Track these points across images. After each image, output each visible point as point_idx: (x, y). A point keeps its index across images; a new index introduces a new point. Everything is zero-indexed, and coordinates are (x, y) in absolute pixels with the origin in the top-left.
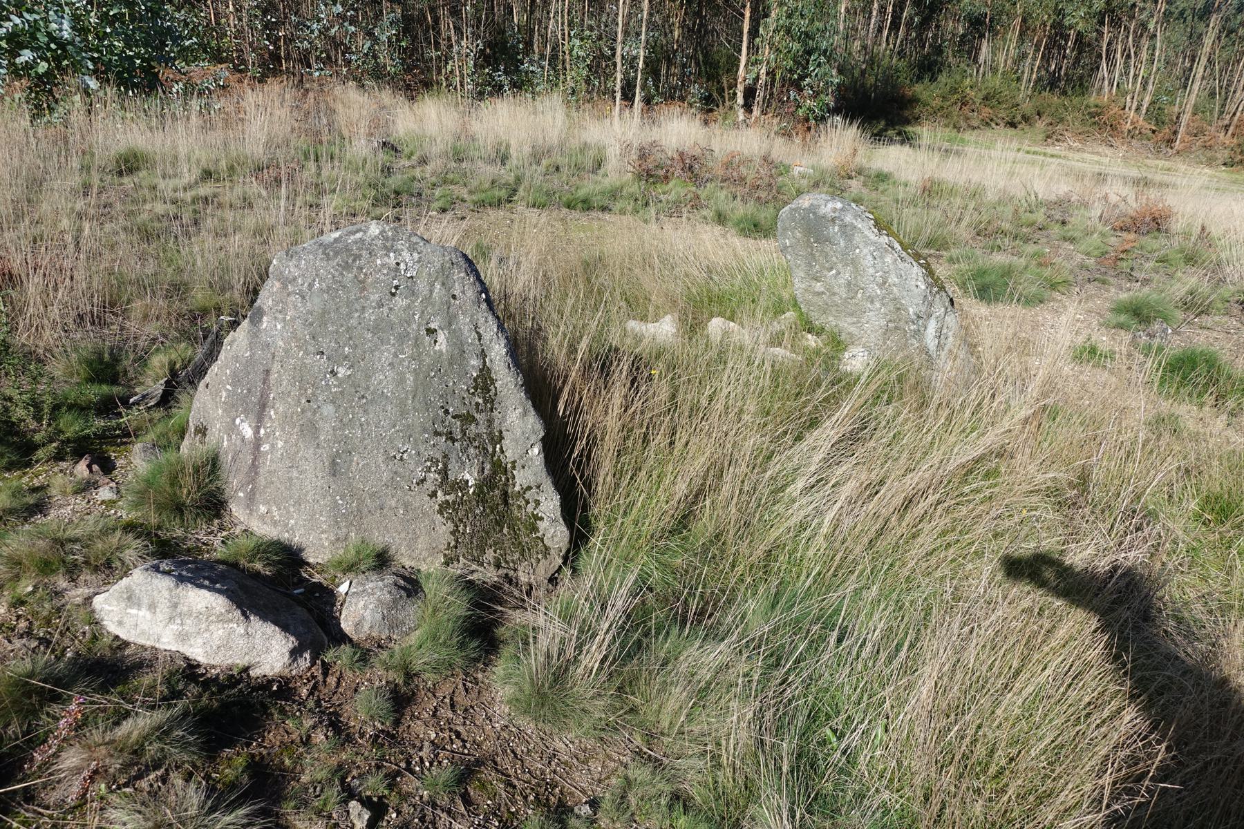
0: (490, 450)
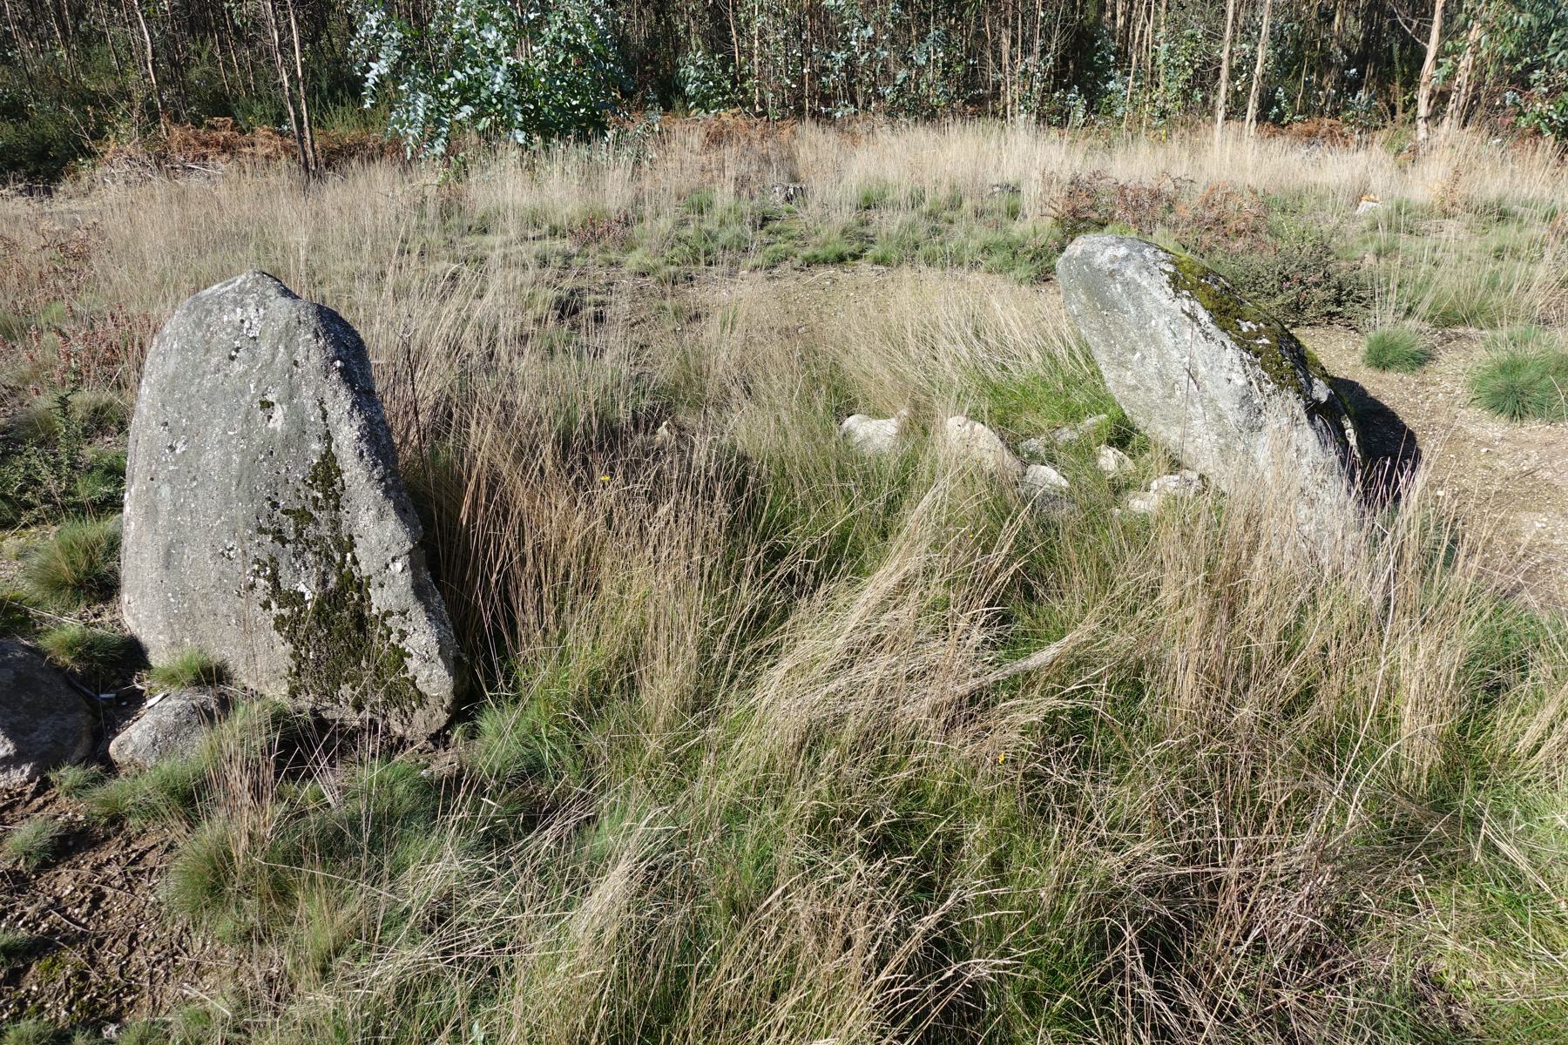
0: (338, 558)
